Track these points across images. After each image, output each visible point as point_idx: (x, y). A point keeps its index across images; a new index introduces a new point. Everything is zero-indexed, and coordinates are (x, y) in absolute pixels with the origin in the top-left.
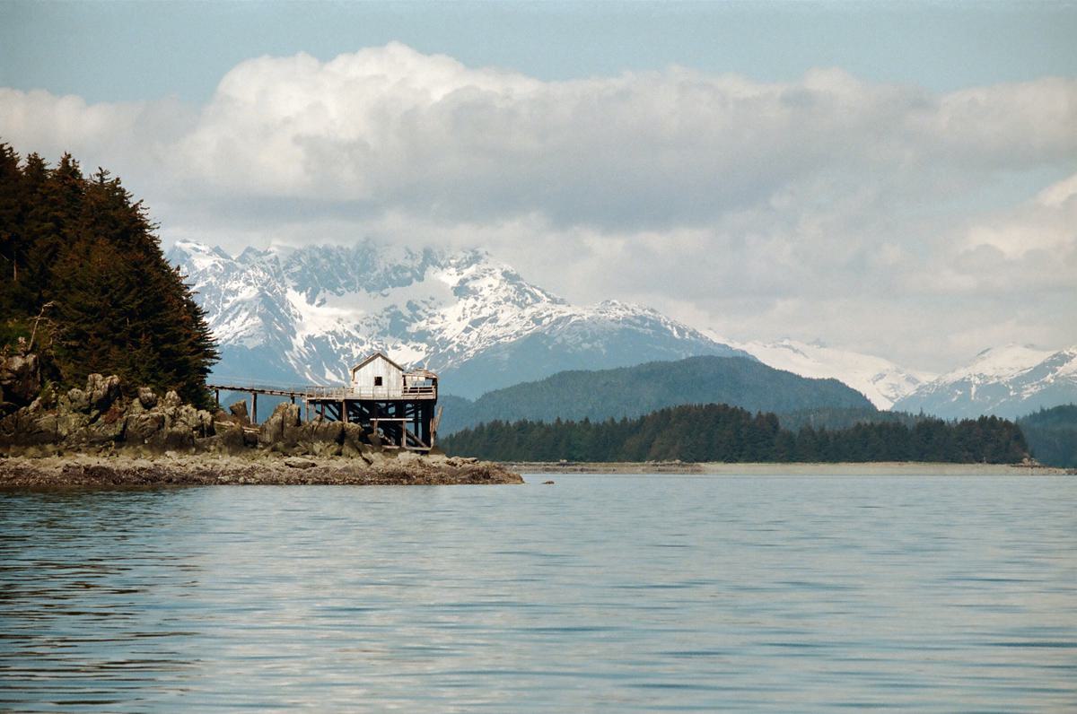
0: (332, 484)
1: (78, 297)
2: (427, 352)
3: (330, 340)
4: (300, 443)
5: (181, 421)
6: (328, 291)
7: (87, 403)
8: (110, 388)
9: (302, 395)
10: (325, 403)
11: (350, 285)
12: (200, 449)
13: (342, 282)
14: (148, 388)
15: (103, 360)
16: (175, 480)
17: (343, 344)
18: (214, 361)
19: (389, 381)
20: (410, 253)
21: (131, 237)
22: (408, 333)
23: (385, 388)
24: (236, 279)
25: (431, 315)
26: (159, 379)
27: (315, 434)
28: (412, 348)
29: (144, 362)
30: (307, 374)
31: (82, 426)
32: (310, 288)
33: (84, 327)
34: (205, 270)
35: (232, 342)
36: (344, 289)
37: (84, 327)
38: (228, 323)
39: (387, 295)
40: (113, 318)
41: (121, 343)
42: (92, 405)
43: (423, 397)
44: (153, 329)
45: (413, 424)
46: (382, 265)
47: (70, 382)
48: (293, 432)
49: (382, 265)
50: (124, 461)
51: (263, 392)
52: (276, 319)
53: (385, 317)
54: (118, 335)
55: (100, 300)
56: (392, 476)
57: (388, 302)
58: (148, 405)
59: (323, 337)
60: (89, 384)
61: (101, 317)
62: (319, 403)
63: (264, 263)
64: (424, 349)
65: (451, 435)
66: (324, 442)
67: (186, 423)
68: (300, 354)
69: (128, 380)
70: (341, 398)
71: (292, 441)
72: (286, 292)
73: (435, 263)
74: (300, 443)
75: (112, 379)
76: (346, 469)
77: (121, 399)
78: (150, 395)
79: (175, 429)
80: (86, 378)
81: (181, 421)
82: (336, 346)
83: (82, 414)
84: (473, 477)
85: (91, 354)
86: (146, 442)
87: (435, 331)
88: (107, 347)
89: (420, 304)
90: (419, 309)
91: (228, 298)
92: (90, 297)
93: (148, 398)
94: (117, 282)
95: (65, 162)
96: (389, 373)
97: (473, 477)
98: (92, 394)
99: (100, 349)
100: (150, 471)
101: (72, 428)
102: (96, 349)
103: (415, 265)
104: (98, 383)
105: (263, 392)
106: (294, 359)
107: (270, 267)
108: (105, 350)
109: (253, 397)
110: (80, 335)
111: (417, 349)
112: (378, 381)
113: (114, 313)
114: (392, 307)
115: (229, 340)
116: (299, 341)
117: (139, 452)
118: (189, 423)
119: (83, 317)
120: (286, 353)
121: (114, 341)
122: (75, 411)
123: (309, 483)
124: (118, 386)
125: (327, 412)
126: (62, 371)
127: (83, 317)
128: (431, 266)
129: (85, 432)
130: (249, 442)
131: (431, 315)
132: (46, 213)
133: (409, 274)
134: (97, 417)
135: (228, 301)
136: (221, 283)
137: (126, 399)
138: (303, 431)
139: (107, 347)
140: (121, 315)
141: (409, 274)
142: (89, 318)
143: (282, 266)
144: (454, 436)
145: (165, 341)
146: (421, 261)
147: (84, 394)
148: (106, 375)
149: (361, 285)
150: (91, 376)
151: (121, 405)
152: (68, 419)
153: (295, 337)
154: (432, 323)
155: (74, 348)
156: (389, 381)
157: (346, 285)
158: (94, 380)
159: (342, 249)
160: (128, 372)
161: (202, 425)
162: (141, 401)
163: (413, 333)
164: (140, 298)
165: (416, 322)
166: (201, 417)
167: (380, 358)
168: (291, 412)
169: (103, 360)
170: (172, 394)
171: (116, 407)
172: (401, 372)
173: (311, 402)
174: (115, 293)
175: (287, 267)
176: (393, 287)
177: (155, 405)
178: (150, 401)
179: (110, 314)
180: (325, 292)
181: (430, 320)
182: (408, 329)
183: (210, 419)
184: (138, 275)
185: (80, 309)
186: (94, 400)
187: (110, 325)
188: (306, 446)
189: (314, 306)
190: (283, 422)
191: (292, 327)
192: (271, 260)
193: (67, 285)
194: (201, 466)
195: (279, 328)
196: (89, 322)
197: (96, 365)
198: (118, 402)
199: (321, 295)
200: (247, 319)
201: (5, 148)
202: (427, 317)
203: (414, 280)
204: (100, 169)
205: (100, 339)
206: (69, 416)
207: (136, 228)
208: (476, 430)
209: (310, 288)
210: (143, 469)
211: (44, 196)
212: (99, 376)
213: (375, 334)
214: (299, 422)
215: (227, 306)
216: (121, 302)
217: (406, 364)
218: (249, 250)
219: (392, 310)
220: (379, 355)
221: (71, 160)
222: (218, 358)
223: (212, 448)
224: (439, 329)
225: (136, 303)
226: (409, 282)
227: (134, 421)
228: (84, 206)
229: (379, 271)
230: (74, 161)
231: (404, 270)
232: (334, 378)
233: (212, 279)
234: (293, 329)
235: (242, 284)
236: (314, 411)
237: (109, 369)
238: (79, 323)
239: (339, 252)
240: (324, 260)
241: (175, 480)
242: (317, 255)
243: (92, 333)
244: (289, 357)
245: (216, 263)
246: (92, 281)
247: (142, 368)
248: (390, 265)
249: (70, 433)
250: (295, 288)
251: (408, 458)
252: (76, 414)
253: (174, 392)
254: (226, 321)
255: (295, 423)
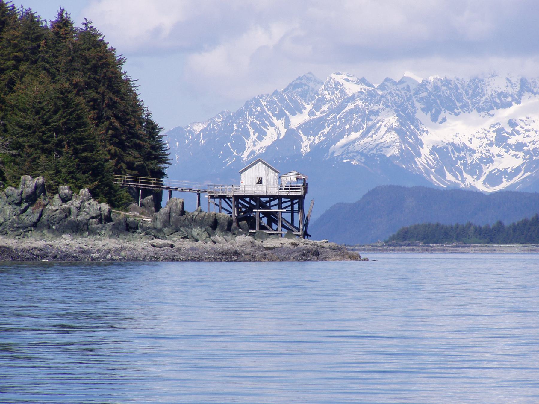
0: (177, 260)
1: (19, 117)
2: (524, 159)
3: (450, 149)
4: (182, 229)
5: (85, 212)
6: (448, 112)
7: (19, 198)
8: (36, 187)
9: (205, 191)
10: (221, 197)
11: (464, 107)
12: (93, 232)
13: (458, 104)
14: (66, 187)
15: (34, 165)
16: (58, 256)
17: (460, 153)
18: (166, 165)
19: (267, 181)
20: (510, 83)
21: (99, 71)
22: (509, 145)
23: (264, 187)
24: (377, 103)
25: (527, 131)
26: (77, 180)
27: (194, 221)
28: (512, 156)
29: (64, 167)
30: (431, 176)
31: (15, 215)
32: (434, 110)
33: (21, 140)
34: (353, 96)
35: (374, 152)
36: (460, 110)
37: (21, 140)
38: (371, 136)
39: (493, 115)
40: (44, 133)
41: (49, 152)
42: (22, 199)
43: (293, 193)
44: (74, 141)
45: (289, 214)
46: (489, 92)
47: (10, 181)
48: (178, 220)
49: (489, 92)
50: (34, 241)
51: (176, 189)
52: (408, 133)
53: (491, 132)
54: (46, 146)
55: (34, 119)
56: (226, 254)
57: (492, 121)
58: (65, 200)
59: (445, 147)
60: (21, 183)
61: (34, 132)
62: (217, 198)
63: (398, 90)
64: (521, 157)
65: (514, 223)
66: (201, 228)
67: (88, 213)
68: (427, 161)
69: (52, 180)
70: (231, 195)
71: (177, 227)
72: (416, 112)
73: (530, 91)
74: (182, 229)
75: (38, 179)
76: (192, 249)
77: (45, 194)
78: (66, 191)
79: (79, 218)
80: (20, 178)
81: (85, 212)
82: (454, 154)
83: (15, 206)
84: (303, 255)
85: (25, 161)
86: (54, 227)
87: (530, 143)
88: (37, 155)
89: (518, 121)
90: (517, 125)
91: (371, 117)
92: (28, 117)
93: (65, 194)
94: (47, 105)
95: (61, 14)
96: (267, 175)
97: (303, 255)
98: (22, 191)
99: (32, 157)
100: (40, 249)
101: (7, 217)
102: (29, 156)
103: (514, 92)
104: (27, 182)
105: (176, 189)
106: (421, 164)
107: (403, 94)
108: (36, 158)
109: (169, 193)
110: (19, 146)
111: (516, 156)
112: (260, 182)
113: (43, 129)
114: (497, 124)
115: (372, 149)
116: (425, 151)
117: (43, 235)
118: (90, 213)
119: (21, 132)
120: (416, 159)
121: (43, 150)
122: (10, 204)
123: (161, 259)
124: (43, 185)
125: (224, 205)
126: (6, 174)
127: (21, 132)
128: (526, 93)
129: (17, 220)
130: (131, 228)
131: (527, 131)
132: (9, 54)
133: (510, 99)
134: (26, 208)
135: (371, 120)
136: (365, 106)
137: (49, 194)
138: (185, 220)
139: (37, 155)
140: (50, 131)
141: (510, 99)
142: (26, 133)
143: (412, 92)
144: (516, 224)
145: (84, 150)
146: (519, 89)
147: (16, 191)
148: (34, 177)
149: (473, 107)
150: (22, 177)
151: (45, 200)
152: (4, 210)
153: (423, 148)
154: (528, 136)
155: (14, 156)
156: (267, 181)
157: (462, 107)
158: (25, 180)
159: (458, 79)
160: (53, 174)
161: (101, 215)
162: (60, 196)
163: (513, 144)
164: (64, 117)
165: (515, 136)
166: (100, 209)
167: (260, 163)
168: (177, 204)
169: (34, 165)
170: (85, 191)
171: (41, 200)
172: (277, 174)
173: (212, 197)
174: (45, 114)
175: (417, 93)
176: (497, 109)
177: (70, 199)
178: (67, 197)
179: (40, 130)
180: (445, 112)
181: (527, 134)
182: (509, 141)
183: (107, 210)
184: (64, 100)
185: (21, 127)
186: (24, 196)
187: (40, 138)
188: (187, 231)
189: (437, 123)
190: (170, 213)
191: (420, 139)
192: (404, 88)
193: (12, 106)
194: (83, 246)
195: (411, 141)
196: (26, 136)
197: (28, 169)
198: (42, 197)
199: (442, 115)
200: (385, 133)
201: (9, 5)
202: (524, 132)
203: (513, 103)
204: (85, 19)
205: (33, 149)
206: (5, 208)
207: (102, 64)
208: (533, 220)
209: (434, 110)
210: (35, 248)
211: (9, 41)
212: (29, 177)
213: (484, 145)
214: (183, 212)
215: (370, 123)
216: (50, 121)
217: (508, 169)
218: (387, 80)
219: (497, 127)
220: (259, 161)
221: (65, 12)
222: (169, 163)
223: (103, 232)
224: (533, 141)
225: (62, 121)
226: (510, 105)
227: (47, 211)
228: (65, 48)
229: (487, 96)
230: (66, 14)
231: (506, 95)
232: (453, 179)
233: (359, 102)
234: (421, 141)
235: (381, 106)
236: (213, 204)
237: (38, 172)
238: (18, 137)
239: (457, 82)
240: (444, 88)
241: (58, 256)
242: (439, 84)
243: (26, 145)
244: (418, 163)
245: (362, 90)
246: (29, 105)
247: (64, 170)
248: (495, 92)
249: (6, 220)
250: (423, 110)
251: (243, 240)
252: (11, 206)
253: (86, 189)
254: (369, 135)
255: (179, 212)
